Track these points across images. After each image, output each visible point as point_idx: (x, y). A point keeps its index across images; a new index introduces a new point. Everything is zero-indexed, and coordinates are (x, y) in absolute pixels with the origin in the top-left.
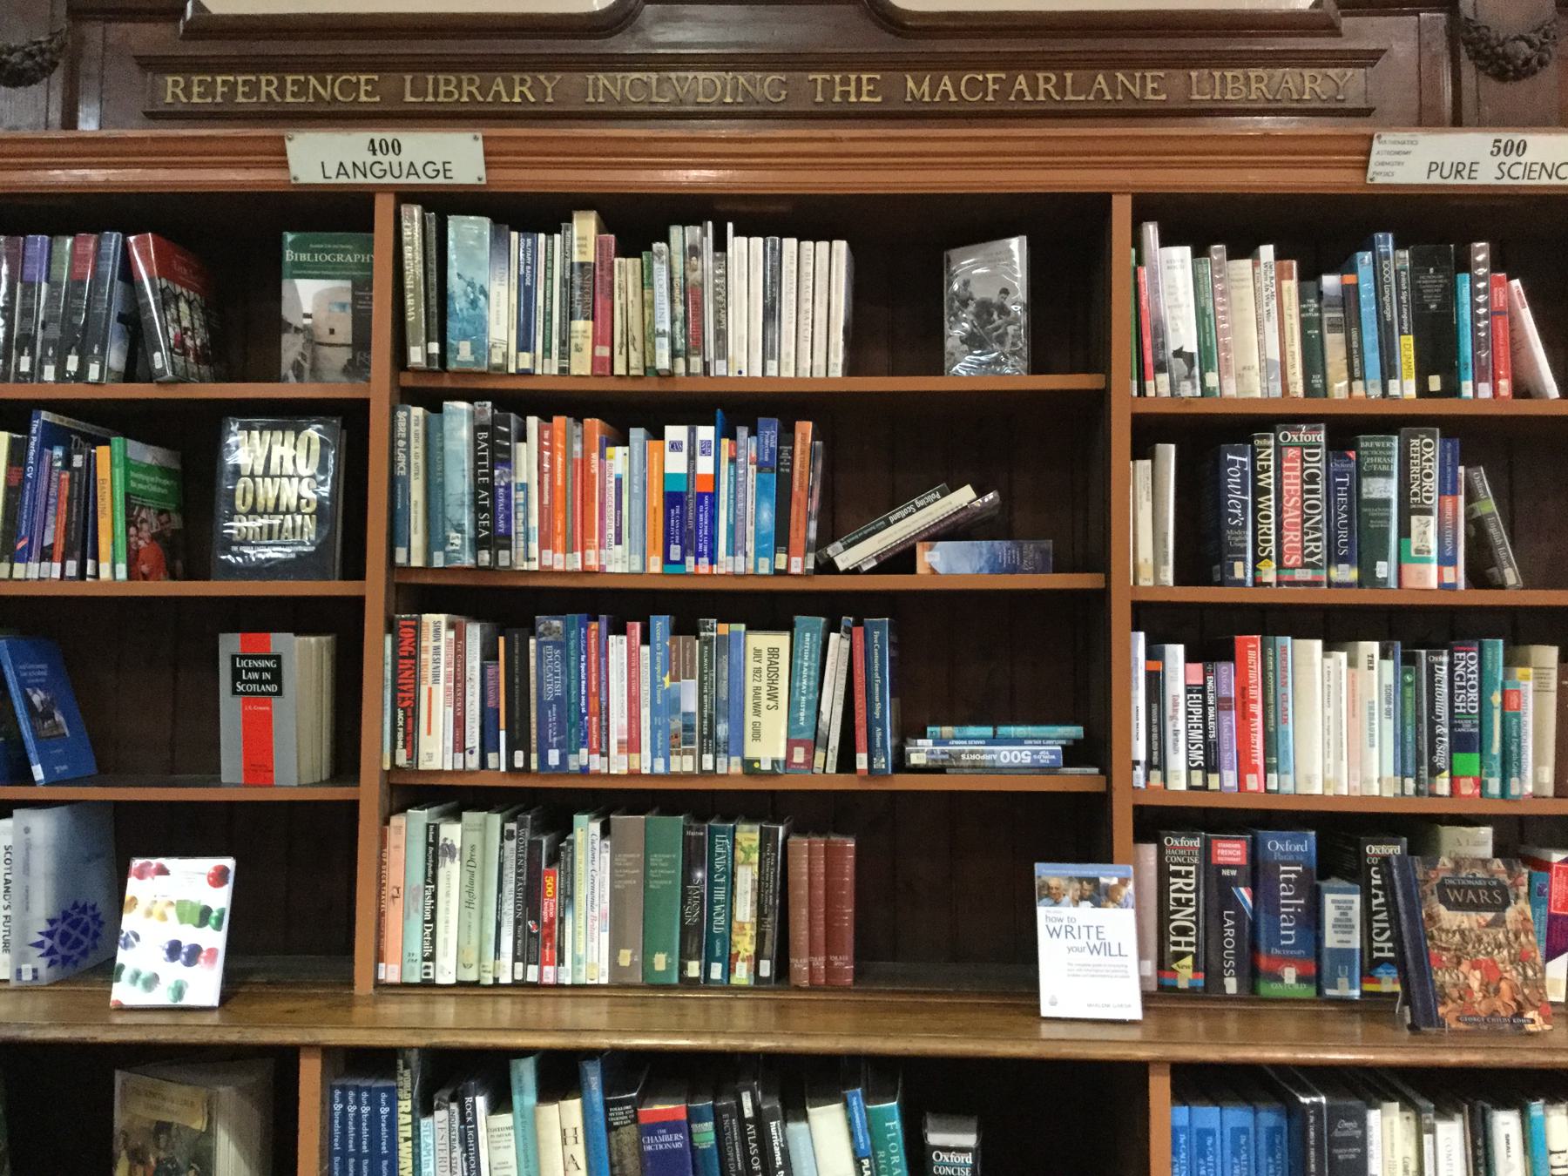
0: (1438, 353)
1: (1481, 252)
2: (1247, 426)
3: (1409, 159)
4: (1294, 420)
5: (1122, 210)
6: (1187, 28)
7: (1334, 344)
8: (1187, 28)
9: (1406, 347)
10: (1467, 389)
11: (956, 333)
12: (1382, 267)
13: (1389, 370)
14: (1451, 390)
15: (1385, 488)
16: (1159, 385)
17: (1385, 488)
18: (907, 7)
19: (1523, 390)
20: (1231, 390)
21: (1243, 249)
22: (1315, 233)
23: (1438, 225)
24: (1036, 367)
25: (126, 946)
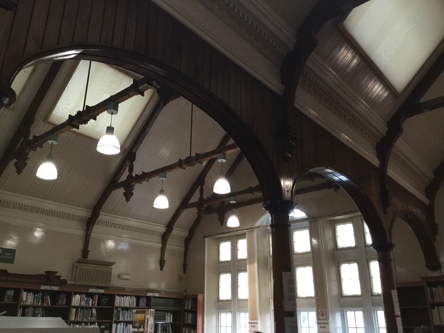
0: (42, 302)
1: (47, 294)
2: (28, 307)
3: (43, 287)
4: (31, 306)
5: (22, 289)
6: (384, 82)
7: (35, 300)
8: (384, 82)
9: (40, 301)
10: (120, 318)
11: (6, 298)
12: (40, 295)
13: (39, 303)
14: (43, 304)
15: (37, 312)
16: (22, 303)
17: (37, 312)
18: (94, 105)
19: (48, 304)
20: (27, 304)
21: (30, 292)
22: (35, 292)
23: (45, 292)
24: (13, 301)
25: (98, 224)
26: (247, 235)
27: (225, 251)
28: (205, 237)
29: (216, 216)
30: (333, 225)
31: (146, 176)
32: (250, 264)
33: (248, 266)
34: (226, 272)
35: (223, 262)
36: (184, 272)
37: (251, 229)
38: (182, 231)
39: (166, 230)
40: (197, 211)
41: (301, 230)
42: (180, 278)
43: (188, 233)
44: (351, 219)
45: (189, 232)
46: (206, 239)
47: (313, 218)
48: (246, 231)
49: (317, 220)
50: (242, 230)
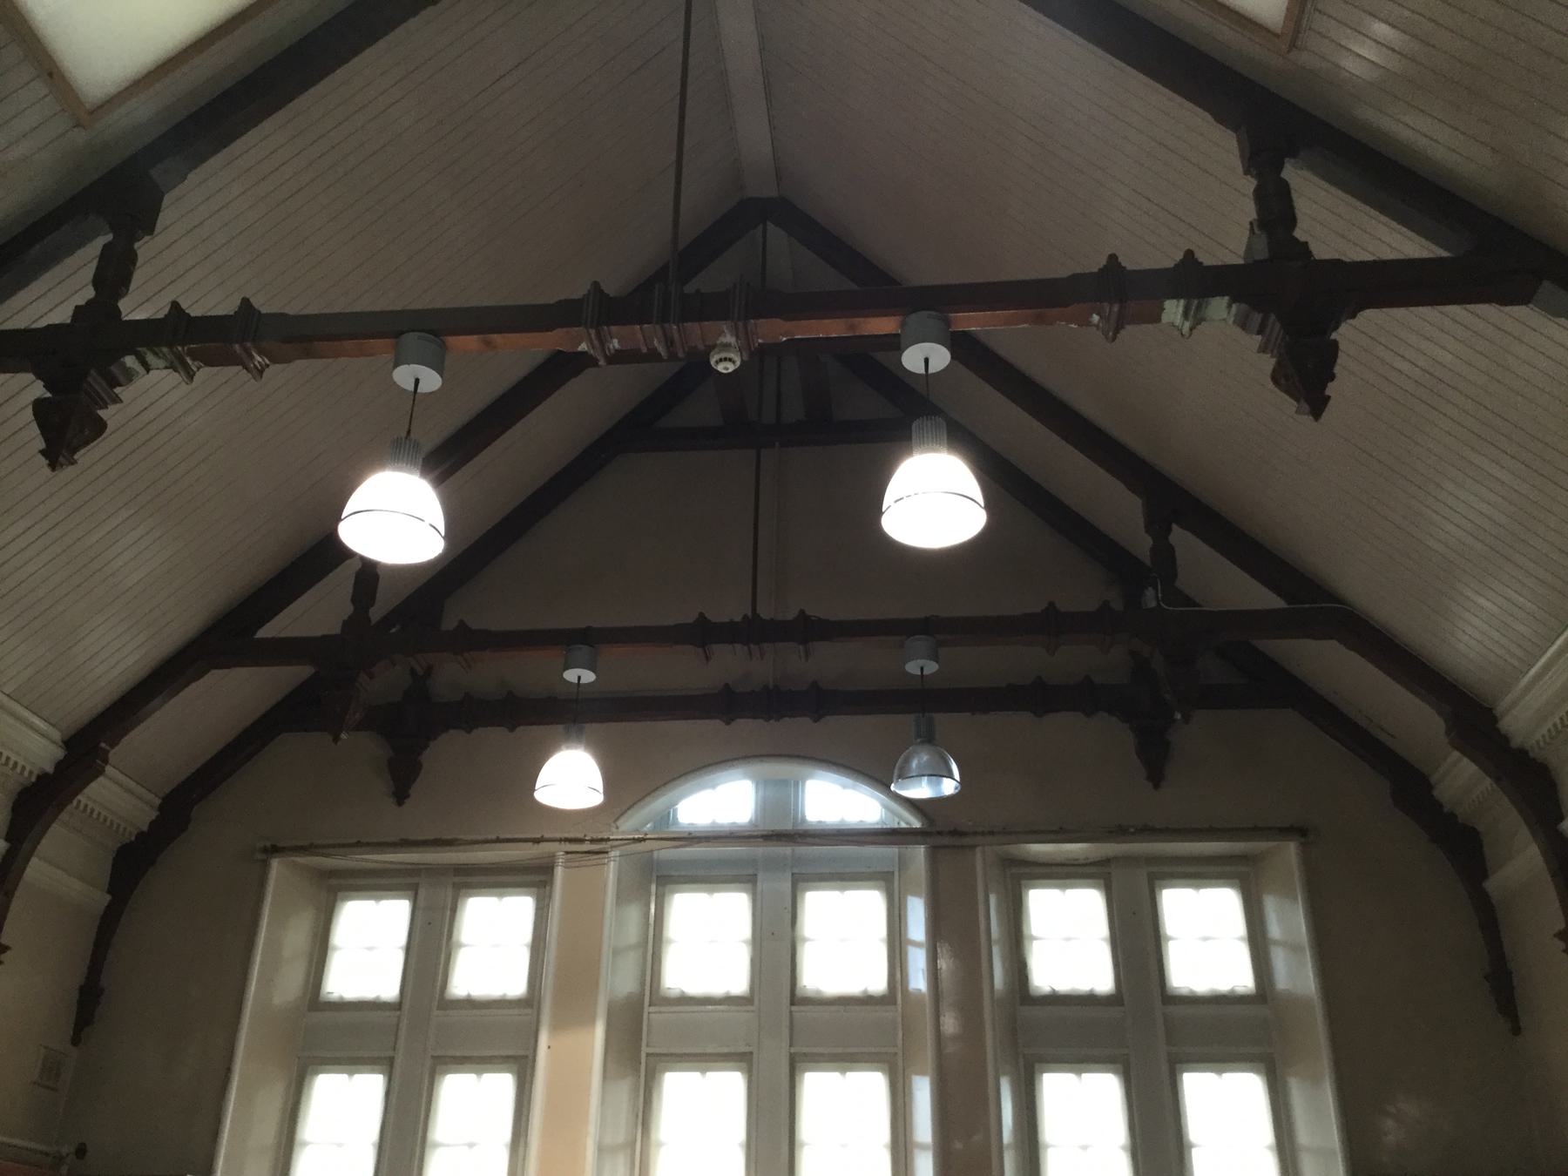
13: (252, 357)
26: (559, 872)
27: (366, 947)
28: (275, 850)
29: (362, 750)
30: (1020, 874)
31: (190, 338)
32: (558, 1026)
33: (544, 1039)
34: (352, 1062)
35: (343, 1006)
36: (76, 1041)
37: (593, 841)
38: (140, 798)
39: (59, 765)
40: (50, 769)
41: (842, 889)
42: (51, 1069)
43: (154, 815)
44: (1094, 870)
45: (161, 808)
46: (276, 865)
47: (955, 833)
48: (559, 849)
49: (973, 847)
50: (537, 841)
